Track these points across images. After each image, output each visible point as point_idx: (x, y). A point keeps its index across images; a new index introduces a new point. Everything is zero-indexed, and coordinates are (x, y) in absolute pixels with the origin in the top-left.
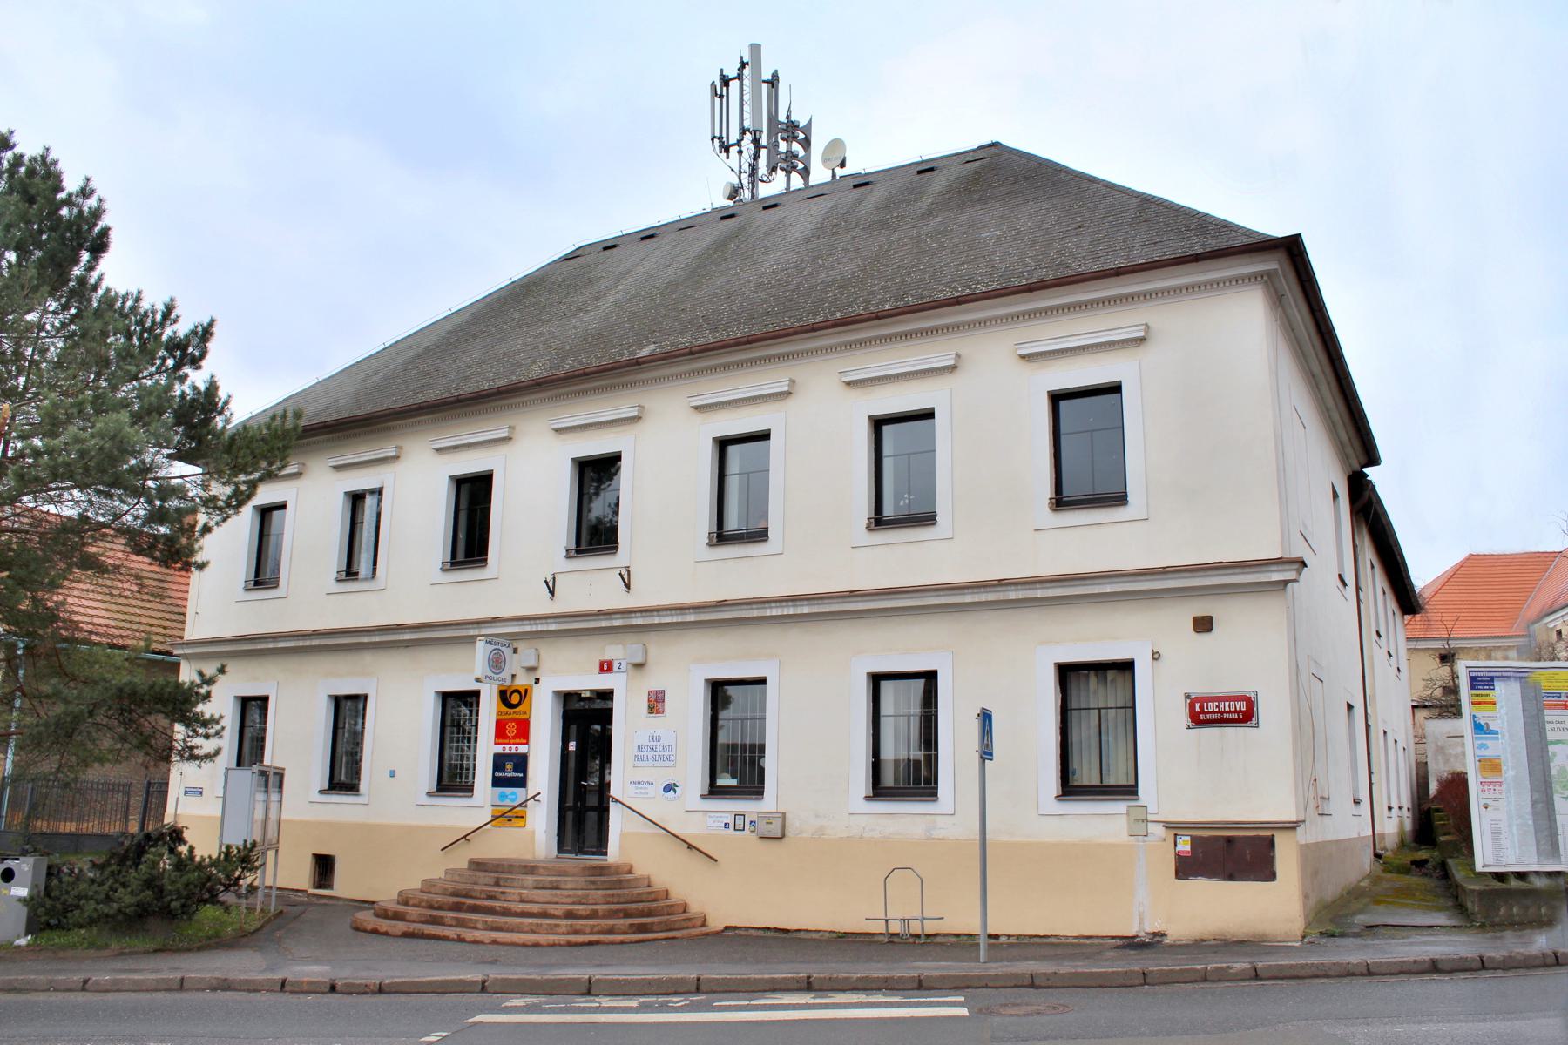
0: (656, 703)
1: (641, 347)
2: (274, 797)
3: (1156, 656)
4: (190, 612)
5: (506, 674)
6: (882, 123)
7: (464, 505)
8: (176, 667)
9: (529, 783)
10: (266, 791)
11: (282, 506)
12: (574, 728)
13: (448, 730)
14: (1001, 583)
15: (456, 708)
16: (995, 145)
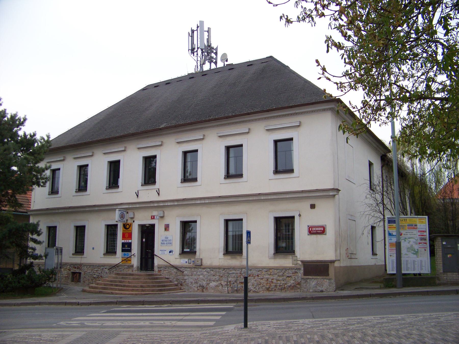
0: (167, 228)
1: (162, 124)
2: (60, 256)
3: (300, 215)
4: (32, 201)
5: (125, 220)
6: (238, 48)
7: (112, 169)
8: (28, 217)
9: (132, 251)
10: (58, 254)
11: (59, 169)
12: (144, 235)
13: (109, 236)
14: (259, 194)
15: (111, 230)
16: (271, 58)
